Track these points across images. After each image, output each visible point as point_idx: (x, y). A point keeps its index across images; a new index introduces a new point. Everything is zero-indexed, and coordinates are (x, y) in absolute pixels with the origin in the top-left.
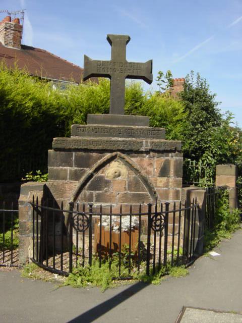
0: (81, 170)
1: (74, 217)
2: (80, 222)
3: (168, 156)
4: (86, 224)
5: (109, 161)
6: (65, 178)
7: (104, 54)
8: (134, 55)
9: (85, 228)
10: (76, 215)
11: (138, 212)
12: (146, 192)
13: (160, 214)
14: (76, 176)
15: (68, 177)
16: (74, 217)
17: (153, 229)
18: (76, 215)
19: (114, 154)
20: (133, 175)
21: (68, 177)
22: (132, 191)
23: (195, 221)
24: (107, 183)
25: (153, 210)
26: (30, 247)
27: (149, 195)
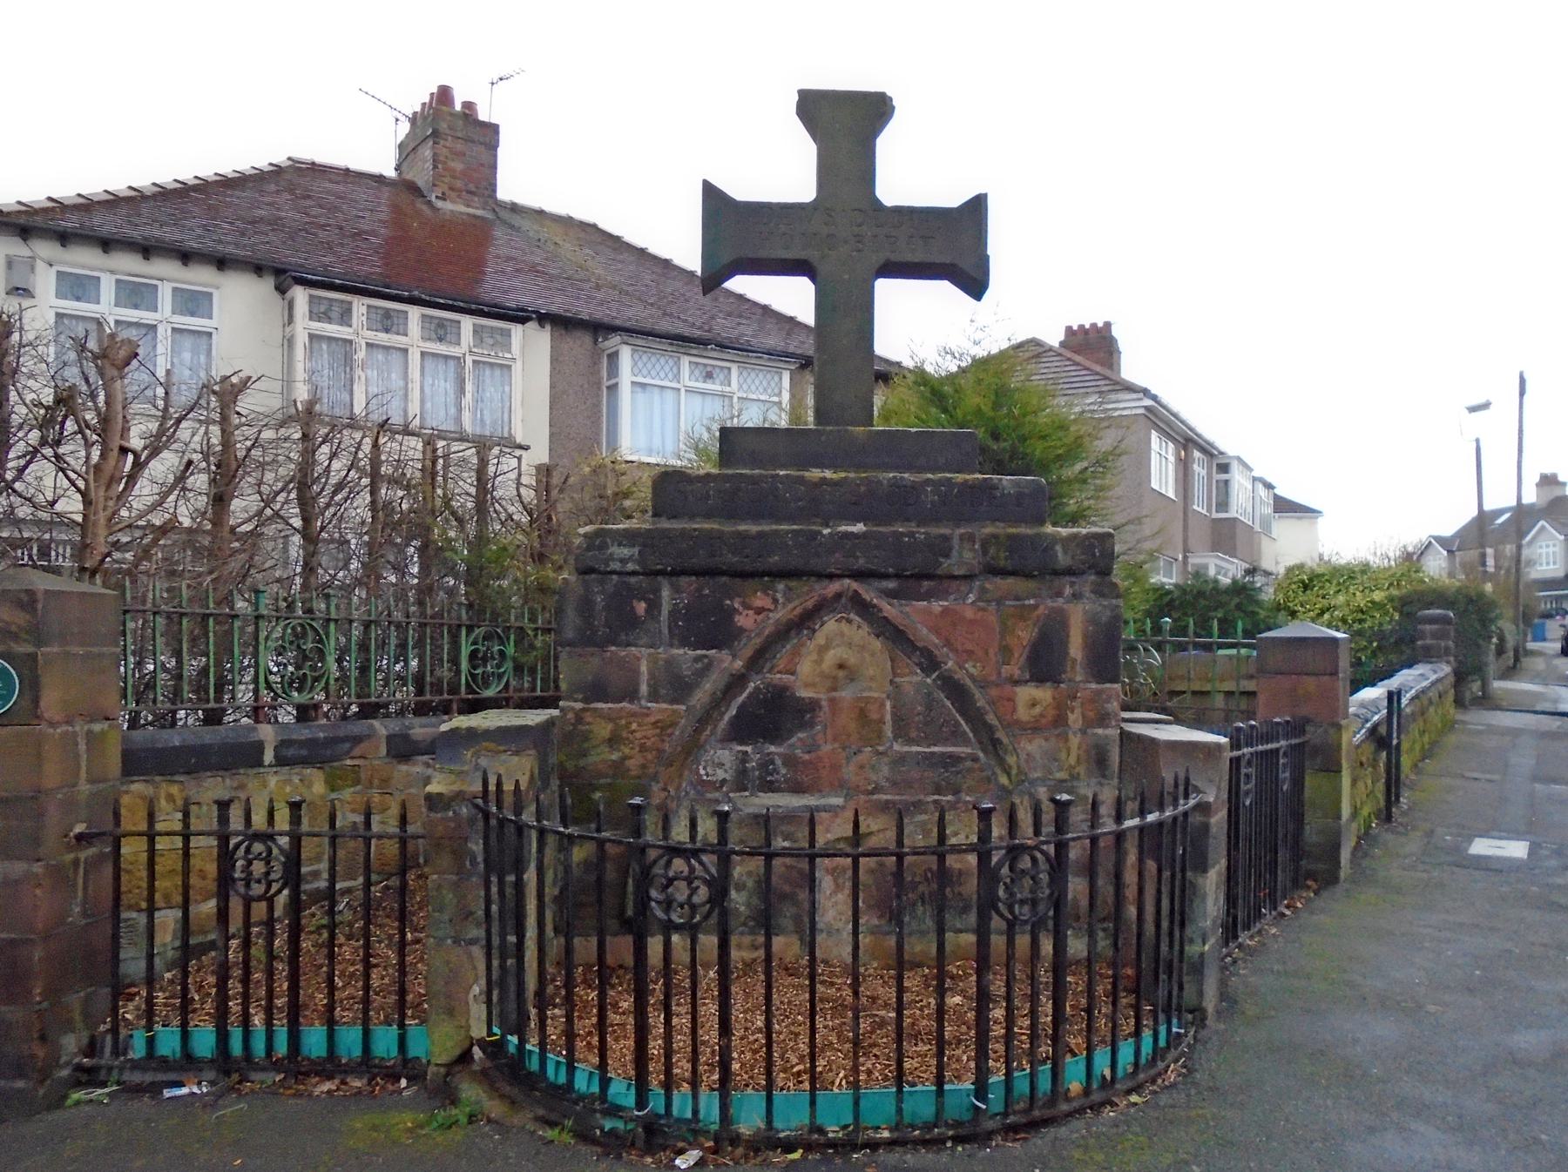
0: (697, 659)
1: (655, 862)
2: (258, 868)
3: (1059, 594)
4: (703, 893)
5: (806, 621)
6: (631, 695)
7: (785, 172)
8: (908, 174)
9: (275, 887)
10: (661, 857)
11: (143, 827)
12: (967, 742)
13: (267, 837)
14: (677, 686)
15: (644, 689)
16: (655, 862)
17: (1002, 916)
18: (661, 857)
19: (834, 587)
20: (914, 680)
21: (644, 689)
22: (910, 741)
23: (1183, 870)
24: (803, 713)
25: (236, 823)
26: (476, 990)
27: (981, 755)
